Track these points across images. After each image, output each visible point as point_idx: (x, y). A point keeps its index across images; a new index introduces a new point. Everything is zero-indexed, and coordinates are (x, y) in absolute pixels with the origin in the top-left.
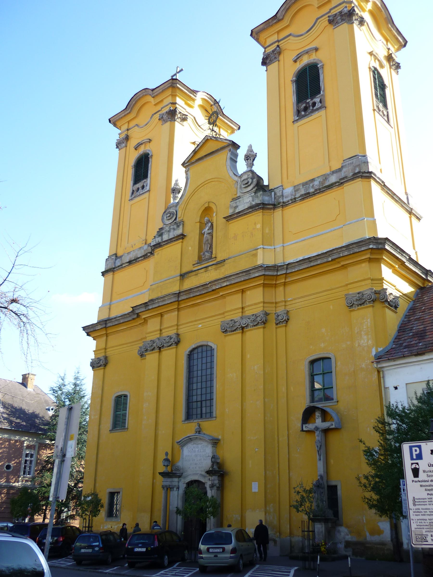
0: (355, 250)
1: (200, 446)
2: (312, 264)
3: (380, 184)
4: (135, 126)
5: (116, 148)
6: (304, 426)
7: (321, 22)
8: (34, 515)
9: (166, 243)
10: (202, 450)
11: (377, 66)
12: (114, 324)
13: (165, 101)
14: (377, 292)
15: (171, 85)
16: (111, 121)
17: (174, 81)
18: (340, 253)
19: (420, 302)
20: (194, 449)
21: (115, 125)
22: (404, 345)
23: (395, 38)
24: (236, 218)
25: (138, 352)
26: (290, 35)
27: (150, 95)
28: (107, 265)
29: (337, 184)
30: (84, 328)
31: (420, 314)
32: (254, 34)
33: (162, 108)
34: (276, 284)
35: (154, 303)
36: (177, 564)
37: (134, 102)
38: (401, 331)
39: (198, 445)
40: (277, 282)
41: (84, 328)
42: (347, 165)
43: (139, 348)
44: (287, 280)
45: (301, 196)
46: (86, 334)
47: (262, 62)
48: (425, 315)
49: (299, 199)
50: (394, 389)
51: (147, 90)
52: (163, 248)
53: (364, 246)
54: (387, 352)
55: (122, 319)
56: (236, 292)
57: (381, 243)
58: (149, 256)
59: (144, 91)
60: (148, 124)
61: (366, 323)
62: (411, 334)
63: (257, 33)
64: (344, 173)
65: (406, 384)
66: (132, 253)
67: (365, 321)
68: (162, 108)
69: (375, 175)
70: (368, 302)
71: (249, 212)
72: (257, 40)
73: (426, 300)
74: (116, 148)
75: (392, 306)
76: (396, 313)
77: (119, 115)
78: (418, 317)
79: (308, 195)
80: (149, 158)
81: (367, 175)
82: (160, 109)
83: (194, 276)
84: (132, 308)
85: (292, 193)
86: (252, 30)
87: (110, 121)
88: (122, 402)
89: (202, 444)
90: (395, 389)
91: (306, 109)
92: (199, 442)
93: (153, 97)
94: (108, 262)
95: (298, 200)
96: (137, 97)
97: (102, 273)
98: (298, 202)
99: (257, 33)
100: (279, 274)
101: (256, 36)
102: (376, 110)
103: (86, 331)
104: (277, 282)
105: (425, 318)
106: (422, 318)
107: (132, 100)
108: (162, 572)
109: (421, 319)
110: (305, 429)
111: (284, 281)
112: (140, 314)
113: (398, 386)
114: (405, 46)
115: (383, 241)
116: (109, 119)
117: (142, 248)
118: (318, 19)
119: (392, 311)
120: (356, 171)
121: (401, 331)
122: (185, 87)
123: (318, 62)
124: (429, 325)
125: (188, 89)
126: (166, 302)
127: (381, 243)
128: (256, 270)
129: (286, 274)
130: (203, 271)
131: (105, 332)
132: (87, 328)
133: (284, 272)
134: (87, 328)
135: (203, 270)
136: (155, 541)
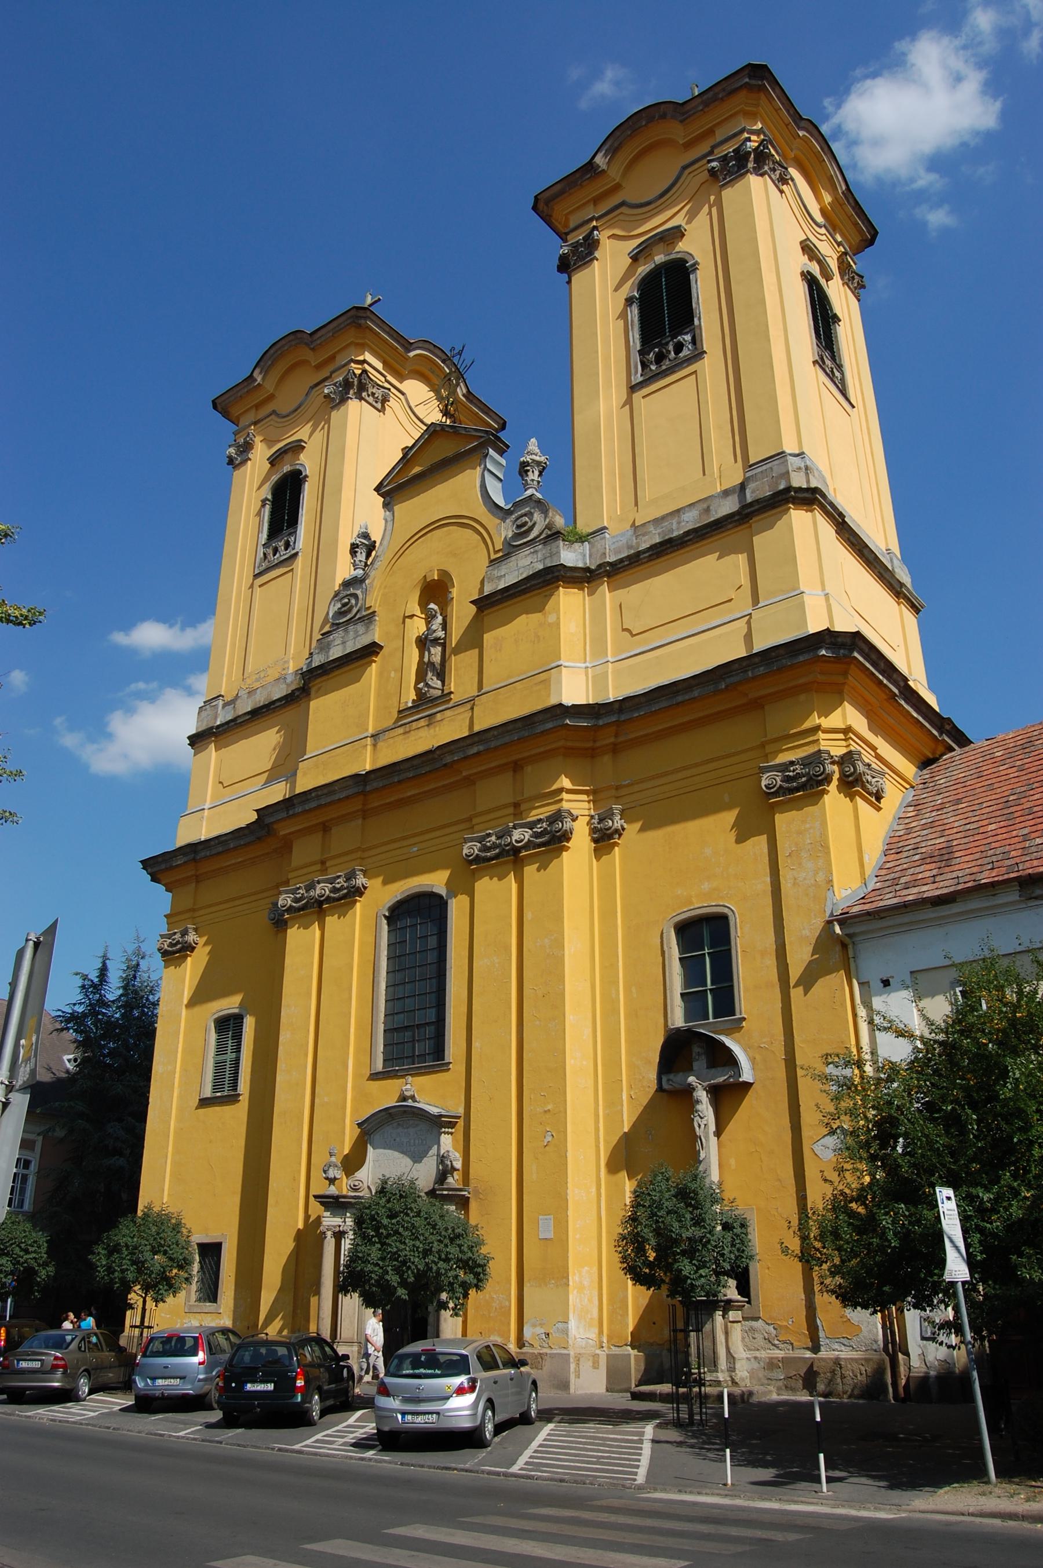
0: (784, 661)
1: (412, 1131)
2: (680, 699)
3: (834, 518)
4: (271, 415)
5: (228, 464)
6: (664, 1079)
7: (692, 175)
8: (273, 498)
9: (337, 664)
10: (417, 1142)
11: (815, 269)
12: (214, 852)
13: (338, 358)
14: (837, 759)
15: (354, 322)
16: (218, 406)
17: (361, 313)
18: (747, 671)
19: (928, 790)
20: (398, 1139)
21: (226, 414)
22: (903, 880)
23: (650, 559)
24: (501, 603)
25: (269, 914)
26: (623, 204)
27: (307, 344)
28: (202, 721)
29: (737, 518)
30: (146, 864)
31: (934, 814)
32: (541, 206)
33: (332, 373)
34: (593, 749)
35: (308, 800)
36: (359, 1413)
37: (270, 363)
38: (893, 851)
39: (408, 1128)
40: (598, 744)
41: (146, 864)
42: (759, 476)
43: (271, 906)
44: (621, 739)
45: (652, 547)
46: (149, 877)
47: (558, 267)
48: (944, 816)
49: (647, 555)
50: (882, 985)
51: (299, 335)
52: (330, 676)
53: (804, 653)
54: (863, 898)
55: (231, 839)
56: (500, 769)
57: (843, 646)
58: (298, 696)
59: (292, 337)
60: (302, 408)
61: (812, 831)
62: (917, 857)
63: (548, 202)
64: (752, 493)
65: (911, 972)
66: (258, 691)
67: (808, 826)
68: (332, 373)
69: (824, 496)
70: (814, 783)
71: (531, 586)
72: (547, 220)
73: (944, 785)
74: (228, 464)
75: (870, 794)
76: (879, 809)
77: (235, 390)
78: (930, 820)
79: (668, 546)
80: (300, 480)
81: (806, 495)
82: (329, 374)
83: (401, 737)
84: (255, 813)
85: (630, 543)
86: (536, 197)
87: (215, 407)
88: (229, 1042)
89: (417, 1125)
90: (889, 985)
91: (660, 358)
92: (411, 1122)
93: (313, 349)
94: (204, 714)
95: (645, 558)
96: (276, 351)
97: (189, 738)
98: (645, 563)
99: (548, 202)
100: (601, 723)
101: (545, 207)
102: (819, 363)
103: (149, 870)
104: (598, 744)
105: (946, 821)
106: (940, 823)
107: (265, 358)
108: (319, 1436)
109: (937, 823)
110: (665, 1086)
111: (612, 740)
112: (275, 826)
113: (893, 977)
114: (871, 242)
115: (848, 641)
116: (214, 402)
117: (282, 680)
118: (684, 168)
119: (871, 803)
120: (782, 487)
121: (893, 851)
122: (385, 327)
123: (687, 258)
124: (959, 835)
125: (392, 332)
126: (336, 797)
127: (843, 646)
128: (549, 715)
129: (617, 723)
130: (423, 724)
131: (193, 873)
132: (152, 862)
133: (614, 719)
134: (152, 862)
135: (422, 723)
136: (910, 580)
